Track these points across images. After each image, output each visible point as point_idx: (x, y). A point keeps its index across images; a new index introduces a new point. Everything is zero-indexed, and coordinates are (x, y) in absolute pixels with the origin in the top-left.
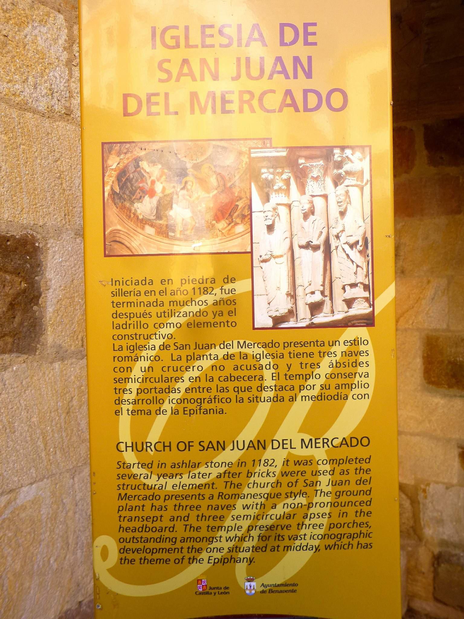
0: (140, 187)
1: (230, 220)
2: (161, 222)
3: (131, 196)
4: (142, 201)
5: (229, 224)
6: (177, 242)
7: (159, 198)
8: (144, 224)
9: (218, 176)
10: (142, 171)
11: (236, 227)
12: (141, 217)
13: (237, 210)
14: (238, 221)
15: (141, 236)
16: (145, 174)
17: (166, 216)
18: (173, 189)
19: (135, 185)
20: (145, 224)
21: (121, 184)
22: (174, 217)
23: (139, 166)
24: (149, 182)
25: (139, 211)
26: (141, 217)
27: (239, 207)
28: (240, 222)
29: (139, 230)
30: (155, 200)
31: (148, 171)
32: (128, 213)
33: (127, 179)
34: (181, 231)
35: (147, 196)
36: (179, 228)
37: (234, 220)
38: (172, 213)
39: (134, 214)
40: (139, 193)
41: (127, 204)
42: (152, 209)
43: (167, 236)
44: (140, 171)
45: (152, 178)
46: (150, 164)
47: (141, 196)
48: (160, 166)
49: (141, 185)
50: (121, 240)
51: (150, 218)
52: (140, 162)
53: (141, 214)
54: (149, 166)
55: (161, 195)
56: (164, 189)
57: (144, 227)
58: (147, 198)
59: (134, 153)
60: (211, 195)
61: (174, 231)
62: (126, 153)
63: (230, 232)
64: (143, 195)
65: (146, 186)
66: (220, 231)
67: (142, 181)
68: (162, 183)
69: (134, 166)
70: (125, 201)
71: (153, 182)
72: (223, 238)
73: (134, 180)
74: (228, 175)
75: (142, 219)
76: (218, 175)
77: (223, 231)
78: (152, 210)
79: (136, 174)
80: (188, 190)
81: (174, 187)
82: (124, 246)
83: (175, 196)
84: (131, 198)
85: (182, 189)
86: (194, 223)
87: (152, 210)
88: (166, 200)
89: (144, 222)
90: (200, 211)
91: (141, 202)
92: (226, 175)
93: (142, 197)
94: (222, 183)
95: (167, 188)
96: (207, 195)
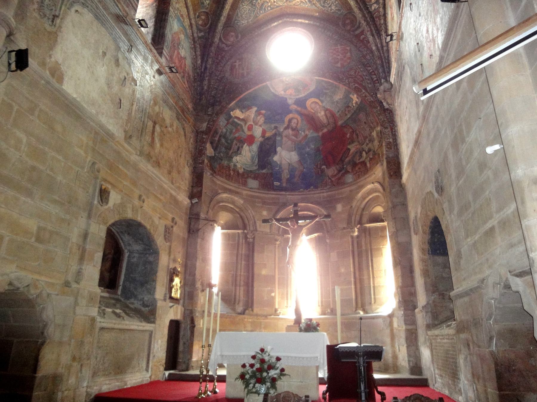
0: (235, 138)
1: (341, 166)
2: (264, 171)
3: (228, 151)
7: (263, 395)
8: (245, 178)
10: (236, 120)
12: (241, 171)
14: (349, 168)
16: (239, 122)
17: (270, 164)
18: (275, 130)
20: (247, 178)
21: (215, 145)
22: (279, 163)
23: (230, 117)
24: (245, 129)
25: (239, 166)
26: (241, 171)
27: (351, 151)
28: (350, 170)
30: (255, 147)
31: (242, 117)
33: (220, 136)
35: (246, 144)
36: (285, 175)
38: (276, 158)
39: (234, 170)
40: (236, 145)
41: (225, 163)
42: (253, 158)
44: (234, 122)
46: (243, 111)
49: (237, 135)
52: (231, 113)
53: (241, 168)
54: (242, 112)
55: (261, 139)
56: (264, 132)
57: (246, 182)
58: (246, 147)
59: (222, 104)
60: (320, 134)
61: (279, 180)
64: (240, 146)
65: (243, 134)
66: (329, 178)
67: (237, 130)
68: (260, 126)
69: (225, 119)
70: (222, 160)
71: (250, 128)
73: (228, 133)
74: (338, 112)
75: (243, 173)
77: (333, 179)
79: (229, 126)
83: (278, 138)
84: (228, 154)
85: (286, 128)
86: (301, 168)
88: (268, 144)
89: (246, 176)
90: (308, 153)
91: (240, 154)
92: (337, 111)
93: (240, 148)
94: (331, 120)
95: (267, 130)
96: (315, 134)
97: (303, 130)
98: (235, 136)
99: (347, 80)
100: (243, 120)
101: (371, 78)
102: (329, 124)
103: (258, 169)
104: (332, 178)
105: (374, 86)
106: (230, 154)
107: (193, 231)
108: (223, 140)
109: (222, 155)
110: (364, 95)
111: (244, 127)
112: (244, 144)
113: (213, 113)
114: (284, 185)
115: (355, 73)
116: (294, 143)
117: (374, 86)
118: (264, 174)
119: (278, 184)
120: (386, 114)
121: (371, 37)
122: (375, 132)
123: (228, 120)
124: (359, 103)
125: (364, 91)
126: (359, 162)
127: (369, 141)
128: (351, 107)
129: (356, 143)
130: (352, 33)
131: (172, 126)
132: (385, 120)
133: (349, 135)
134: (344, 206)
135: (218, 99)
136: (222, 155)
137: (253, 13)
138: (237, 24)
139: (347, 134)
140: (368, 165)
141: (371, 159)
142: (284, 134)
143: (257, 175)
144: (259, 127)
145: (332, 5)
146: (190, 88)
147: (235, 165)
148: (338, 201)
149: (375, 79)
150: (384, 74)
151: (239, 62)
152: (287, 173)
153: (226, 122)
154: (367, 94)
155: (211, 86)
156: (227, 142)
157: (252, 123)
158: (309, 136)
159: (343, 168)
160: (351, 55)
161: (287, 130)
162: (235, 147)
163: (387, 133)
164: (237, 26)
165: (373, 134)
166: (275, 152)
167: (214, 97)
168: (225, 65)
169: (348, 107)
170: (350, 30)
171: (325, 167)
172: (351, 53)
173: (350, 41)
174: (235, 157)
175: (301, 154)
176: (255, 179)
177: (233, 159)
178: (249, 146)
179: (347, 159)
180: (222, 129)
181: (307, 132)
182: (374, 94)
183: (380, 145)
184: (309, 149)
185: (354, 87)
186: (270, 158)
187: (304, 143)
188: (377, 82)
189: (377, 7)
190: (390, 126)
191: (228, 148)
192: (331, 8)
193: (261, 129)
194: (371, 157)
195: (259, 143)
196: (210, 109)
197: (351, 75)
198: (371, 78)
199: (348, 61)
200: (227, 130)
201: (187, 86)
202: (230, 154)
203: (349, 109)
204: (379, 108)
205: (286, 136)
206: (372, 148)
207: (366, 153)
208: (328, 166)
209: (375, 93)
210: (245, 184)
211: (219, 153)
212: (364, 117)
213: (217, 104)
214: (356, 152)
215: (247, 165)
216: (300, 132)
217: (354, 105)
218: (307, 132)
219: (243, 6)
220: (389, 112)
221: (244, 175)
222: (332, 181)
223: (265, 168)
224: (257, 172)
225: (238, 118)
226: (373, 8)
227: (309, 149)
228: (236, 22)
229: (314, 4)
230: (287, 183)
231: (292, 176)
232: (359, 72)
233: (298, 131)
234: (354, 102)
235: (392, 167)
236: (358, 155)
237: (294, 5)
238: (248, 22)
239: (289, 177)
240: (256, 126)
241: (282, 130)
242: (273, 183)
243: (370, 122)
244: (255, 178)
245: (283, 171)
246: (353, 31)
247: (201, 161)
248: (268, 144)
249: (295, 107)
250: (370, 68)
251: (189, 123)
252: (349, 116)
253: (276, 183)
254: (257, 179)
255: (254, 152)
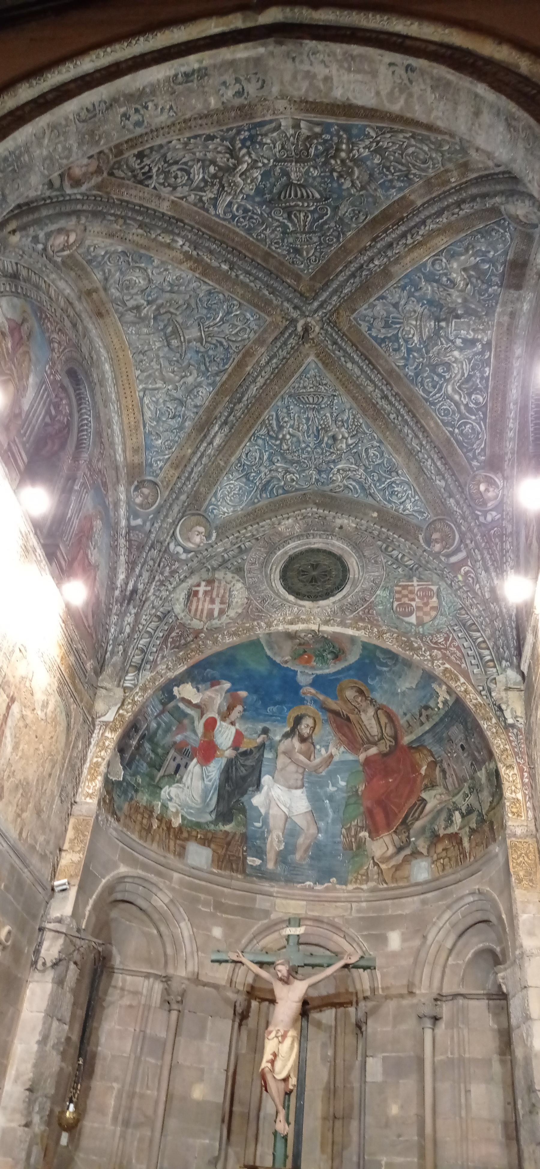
0: (175, 743)
1: (404, 837)
2: (228, 828)
4: (182, 778)
5: (400, 849)
6: (266, 886)
9: (379, 712)
10: (181, 705)
11: (414, 862)
12: (177, 822)
13: (421, 812)
14: (422, 845)
15: (176, 875)
16: (189, 711)
17: (243, 811)
19: (162, 743)
20: (187, 839)
21: (127, 756)
22: (263, 811)
25: (172, 807)
26: (177, 822)
27: (428, 807)
28: (424, 851)
29: (172, 859)
32: (145, 821)
33: (143, 737)
34: (279, 854)
37: (413, 839)
38: (258, 800)
39: (160, 819)
40: (174, 759)
42: (205, 792)
43: (242, 868)
44: (177, 708)
45: (208, 715)
46: (200, 686)
47: (178, 767)
48: (227, 685)
49: (178, 738)
50: (127, 897)
51: (202, 820)
54: (198, 690)
55: (230, 753)
56: (239, 736)
57: (184, 848)
58: (194, 766)
60: (362, 757)
61: (260, 853)
62: (138, 668)
63: (399, 874)
64: (183, 764)
66: (375, 864)
67: (181, 728)
68: (233, 723)
69: (160, 701)
70: (137, 791)
72: (381, 886)
73: (160, 732)
75: (180, 827)
76: (379, 709)
77: (383, 866)
78: (206, 797)
80: (303, 740)
81: (265, 731)
82: (134, 908)
83: (268, 755)
84: (152, 778)
85: (286, 736)
87: (206, 797)
88: (243, 766)
89: (185, 835)
91: (180, 781)
93: (182, 768)
95: (245, 733)
96: (350, 757)
97: (323, 744)
98: (174, 740)
99: (428, 653)
100: (197, 706)
101: (480, 654)
102: (382, 738)
103: (215, 822)
104: (383, 863)
105: (486, 672)
106: (157, 779)
107: (44, 964)
108: (147, 746)
109: (140, 780)
110: (463, 689)
111: (196, 723)
112: (192, 759)
113: (135, 686)
114: (270, 866)
115: (446, 639)
116: (301, 770)
117: (486, 672)
118: (226, 833)
119: (258, 862)
120: (509, 737)
121: (483, 572)
122: (483, 769)
123: (164, 704)
124: (450, 703)
125: (462, 680)
126: (445, 835)
127: (470, 788)
128: (432, 709)
129: (440, 790)
130: (443, 559)
131: (45, 705)
132: (507, 750)
133: (425, 768)
134: (404, 940)
135: (151, 658)
136: (140, 780)
137: (247, 497)
138: (212, 512)
139: (421, 767)
140: (466, 844)
141: (473, 831)
142: (282, 747)
143: (210, 835)
144: (230, 726)
145: (408, 501)
146: (95, 628)
147: (165, 807)
148: (393, 922)
149: (488, 658)
150: (507, 652)
151: (206, 586)
152: (278, 837)
153: (160, 707)
154: (470, 688)
155: (141, 627)
156: (153, 751)
157: (216, 716)
158: (336, 759)
159: (409, 843)
160: (440, 603)
161: (290, 739)
162: (170, 765)
163: (511, 779)
164: (212, 516)
165: (479, 774)
166: (258, 786)
167: (142, 651)
168: (174, 588)
169: (427, 708)
170: (439, 553)
171: (366, 834)
172: (438, 597)
173: (438, 575)
174: (167, 787)
175: (315, 799)
176: (204, 845)
177: (162, 792)
178: (202, 766)
179: (418, 824)
180: (150, 722)
181: (333, 750)
182: (484, 690)
183: (494, 804)
184: (335, 789)
185: (442, 668)
186: (245, 799)
187: (324, 774)
188: (491, 664)
189: (497, 518)
190: (519, 763)
191: (156, 765)
192: (404, 507)
193: (233, 730)
194: (474, 826)
195: (224, 761)
196: (130, 676)
197: (436, 643)
198: (480, 654)
199: (433, 613)
200: (159, 725)
201: (91, 624)
202: (157, 779)
203: (429, 712)
204: (494, 721)
205: (285, 753)
206: (476, 805)
207: (463, 816)
208: (375, 832)
209: (486, 688)
210: (181, 854)
211: (134, 775)
212: (461, 736)
213: (148, 666)
214: (439, 812)
215: (191, 808)
216: (318, 747)
217: (441, 705)
218: (333, 750)
219: (229, 479)
220: (515, 731)
221: (182, 833)
222: (381, 872)
223: (230, 821)
224: (212, 827)
225: (188, 703)
226: (489, 518)
227: (335, 789)
228: (211, 507)
229: (370, 494)
230: (276, 863)
231: (290, 849)
232: (454, 639)
233: (313, 743)
234: (441, 699)
235: (521, 859)
236: (444, 815)
237: (331, 490)
238: (234, 511)
239: (282, 847)
240: (224, 724)
241: (278, 738)
242: (245, 858)
243: (473, 747)
244: (206, 842)
245: (269, 832)
246: (448, 556)
247: (90, 791)
248: (243, 766)
249: (313, 691)
250: (478, 634)
251: (82, 701)
252: (427, 728)
253: (253, 861)
254: (209, 846)
255: (210, 781)
